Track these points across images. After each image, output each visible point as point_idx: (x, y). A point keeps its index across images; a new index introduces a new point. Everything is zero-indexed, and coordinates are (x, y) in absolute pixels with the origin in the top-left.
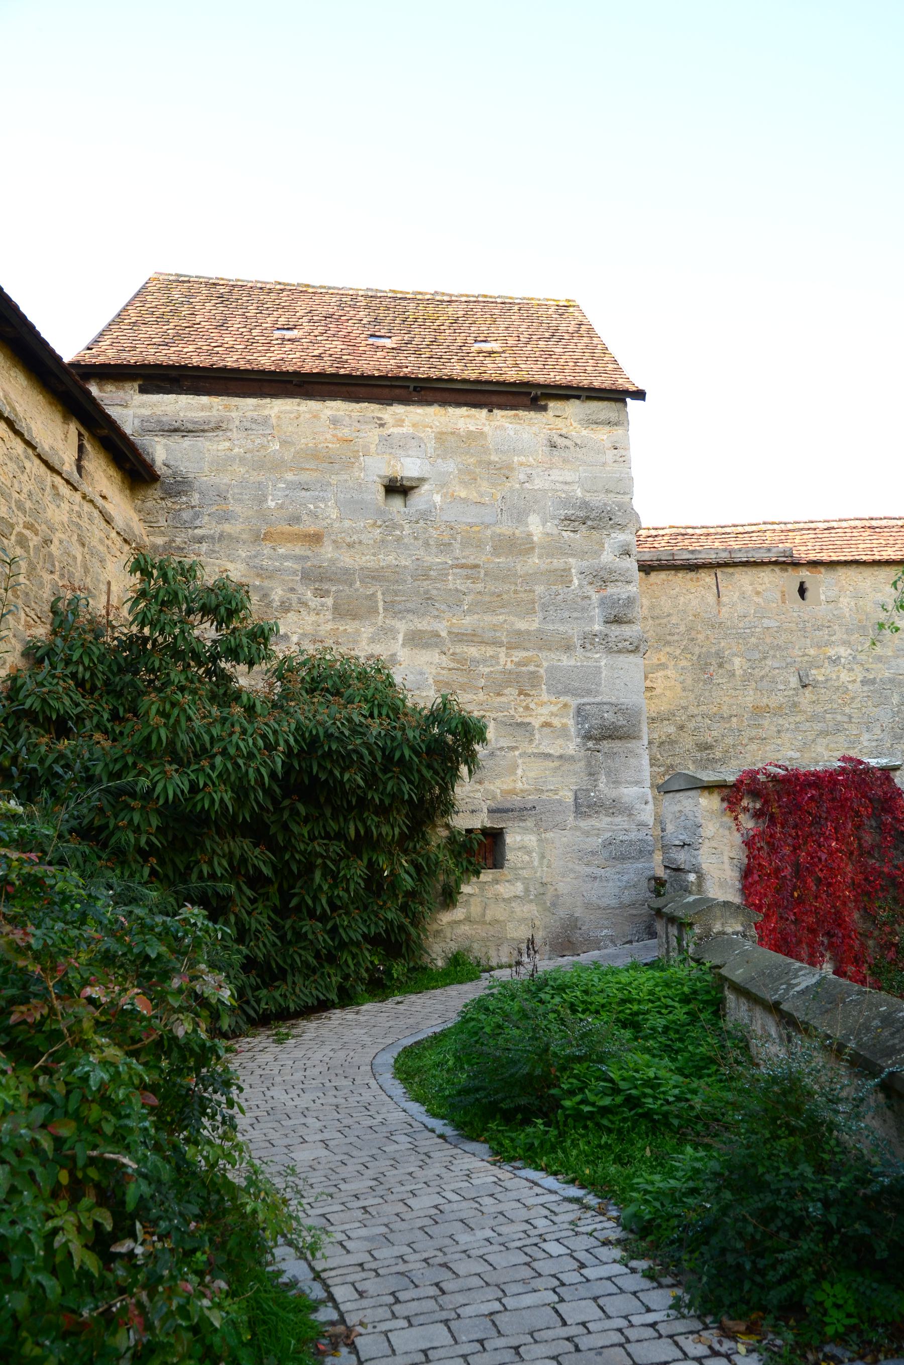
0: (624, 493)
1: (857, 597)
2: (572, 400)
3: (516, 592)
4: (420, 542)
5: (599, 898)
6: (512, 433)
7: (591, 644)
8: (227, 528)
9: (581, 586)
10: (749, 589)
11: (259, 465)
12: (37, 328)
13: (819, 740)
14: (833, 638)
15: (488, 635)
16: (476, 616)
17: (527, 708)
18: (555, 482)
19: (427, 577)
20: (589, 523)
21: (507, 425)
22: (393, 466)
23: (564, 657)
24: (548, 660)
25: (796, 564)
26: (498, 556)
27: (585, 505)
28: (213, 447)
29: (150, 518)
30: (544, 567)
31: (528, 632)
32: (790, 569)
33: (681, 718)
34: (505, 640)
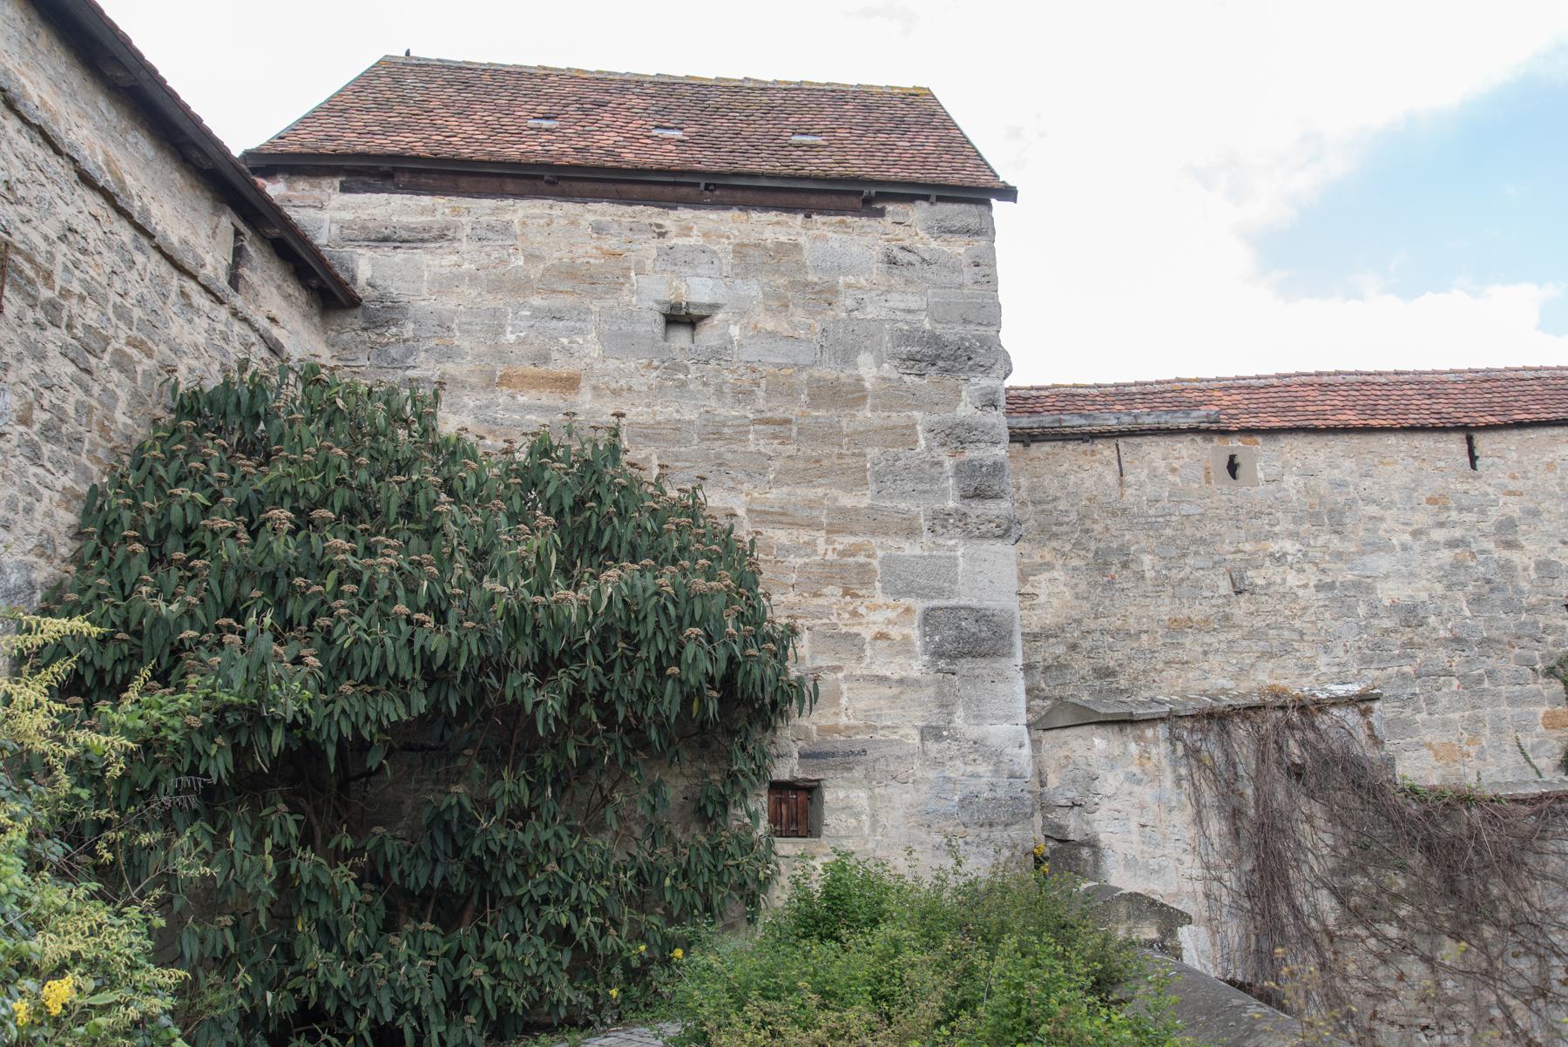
0: (989, 324)
2: (918, 203)
3: (840, 456)
4: (711, 389)
6: (836, 245)
7: (943, 527)
9: (929, 449)
10: (1161, 465)
11: (496, 286)
12: (162, 73)
13: (1261, 664)
14: (1277, 529)
15: (803, 514)
16: (785, 489)
17: (855, 613)
18: (893, 310)
19: (719, 435)
20: (941, 363)
21: (830, 234)
22: (677, 288)
23: (906, 545)
24: (881, 548)
25: (1224, 433)
26: (817, 407)
27: (935, 339)
28: (433, 262)
29: (346, 354)
30: (878, 422)
31: (856, 510)
32: (1216, 439)
33: (1073, 634)
34: (824, 520)
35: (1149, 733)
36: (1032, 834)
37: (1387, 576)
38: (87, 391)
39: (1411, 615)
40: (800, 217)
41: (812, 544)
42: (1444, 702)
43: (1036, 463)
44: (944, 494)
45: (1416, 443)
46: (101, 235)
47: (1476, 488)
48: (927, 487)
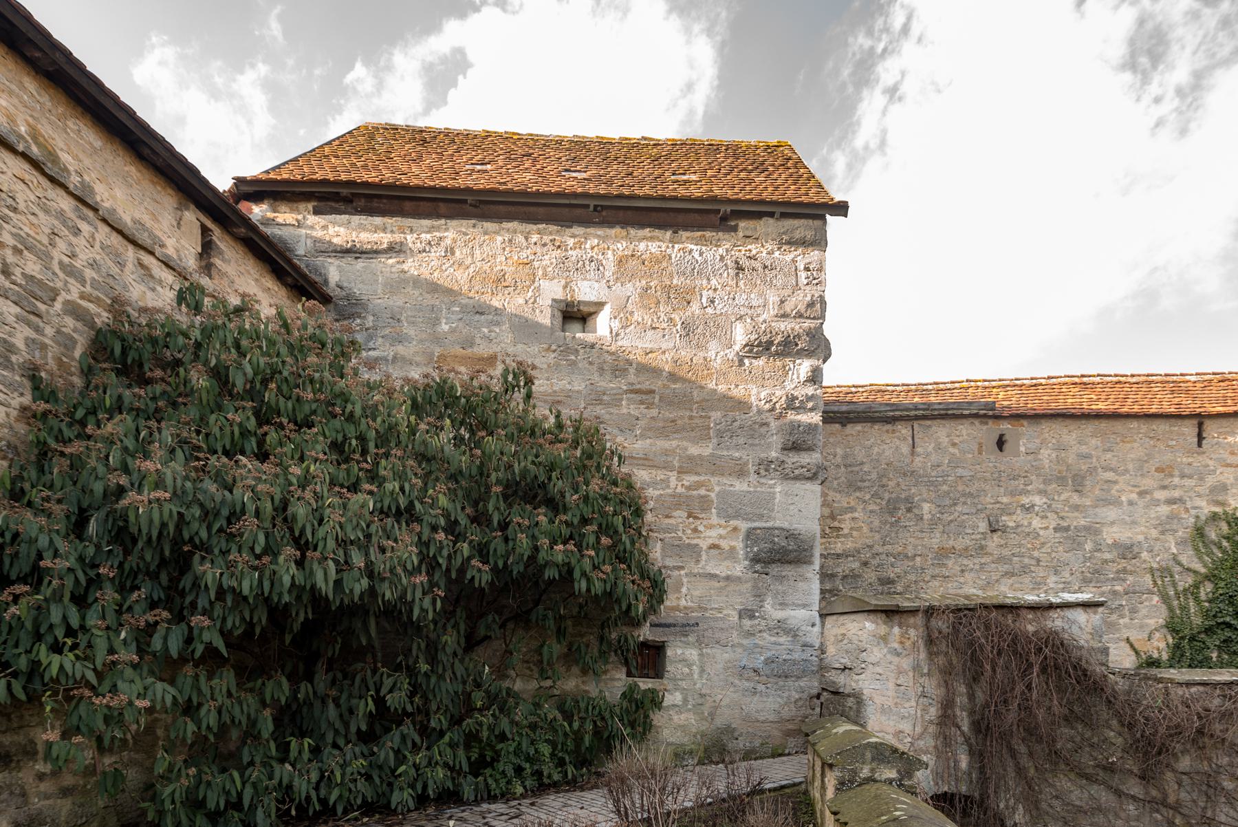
1: (1061, 448)
3: (691, 418)
4: (595, 367)
5: (757, 711)
7: (766, 470)
8: (400, 349)
10: (945, 440)
13: (1004, 580)
14: (1029, 488)
16: (648, 441)
17: (695, 530)
19: (599, 401)
24: (717, 485)
32: (990, 422)
35: (912, 620)
36: (814, 685)
37: (1113, 523)
38: (37, 330)
39: (1127, 551)
40: (669, 234)
41: (666, 482)
42: (1144, 612)
43: (850, 438)
44: (769, 446)
45: (1154, 427)
46: (32, 198)
47: (1197, 461)
48: (757, 441)
